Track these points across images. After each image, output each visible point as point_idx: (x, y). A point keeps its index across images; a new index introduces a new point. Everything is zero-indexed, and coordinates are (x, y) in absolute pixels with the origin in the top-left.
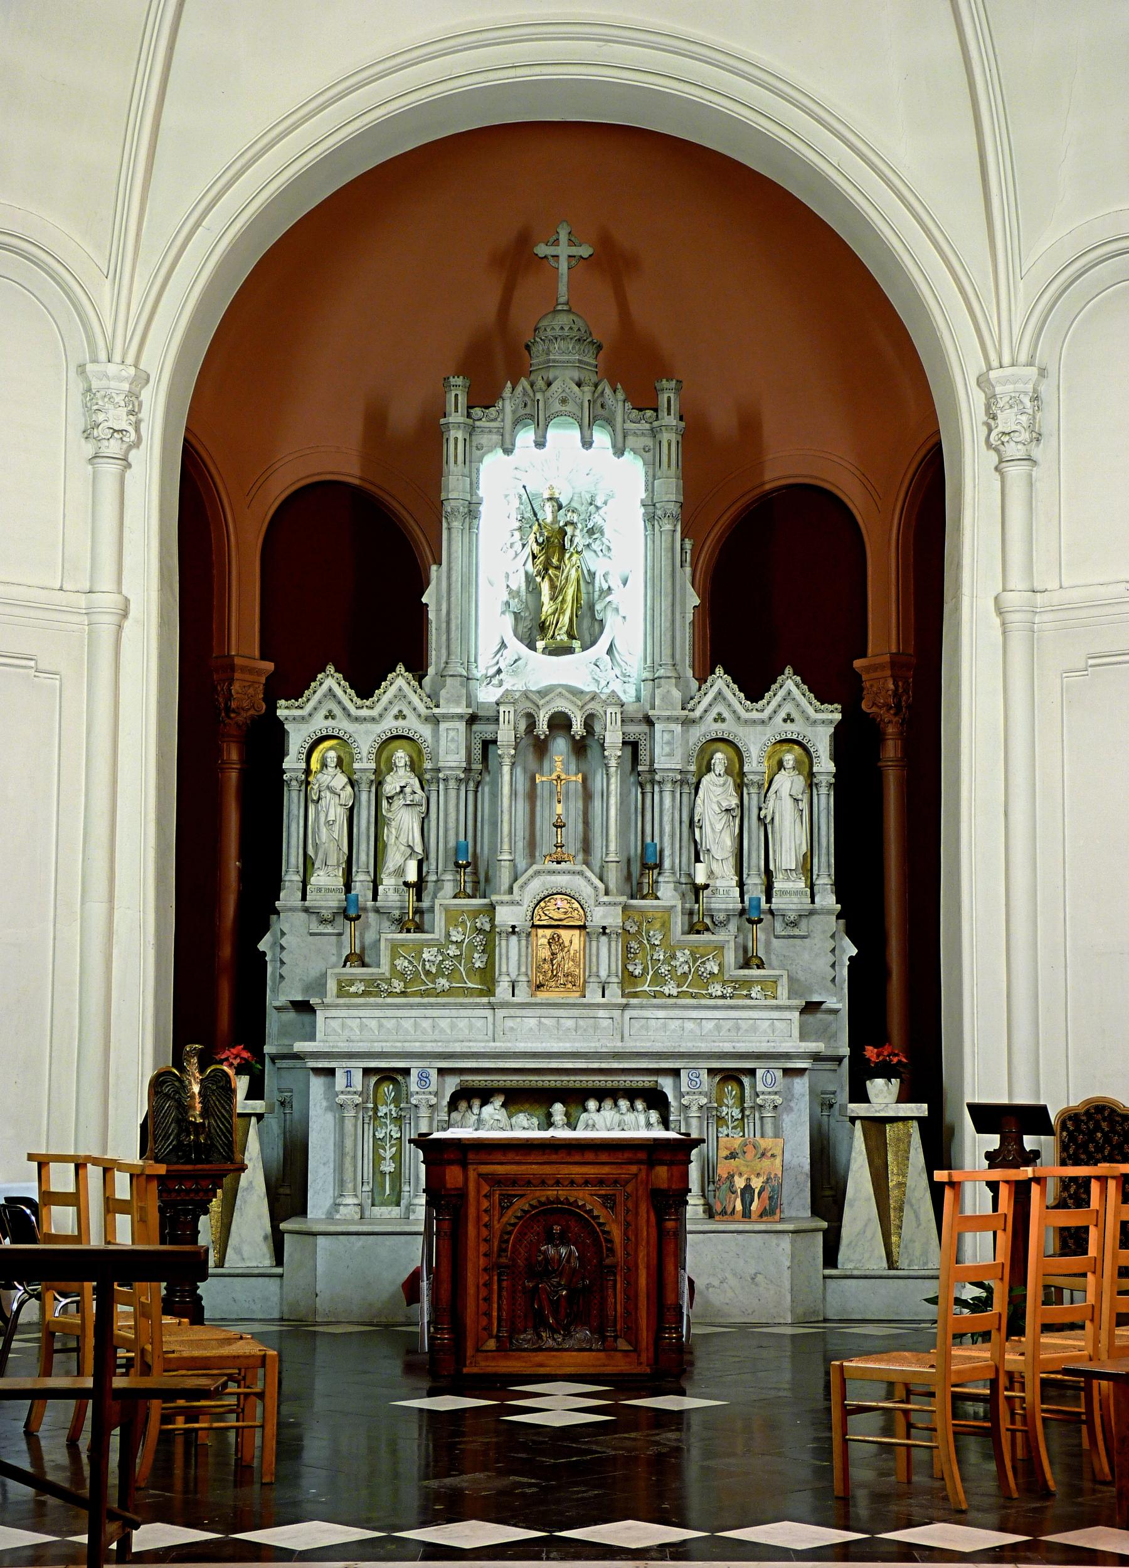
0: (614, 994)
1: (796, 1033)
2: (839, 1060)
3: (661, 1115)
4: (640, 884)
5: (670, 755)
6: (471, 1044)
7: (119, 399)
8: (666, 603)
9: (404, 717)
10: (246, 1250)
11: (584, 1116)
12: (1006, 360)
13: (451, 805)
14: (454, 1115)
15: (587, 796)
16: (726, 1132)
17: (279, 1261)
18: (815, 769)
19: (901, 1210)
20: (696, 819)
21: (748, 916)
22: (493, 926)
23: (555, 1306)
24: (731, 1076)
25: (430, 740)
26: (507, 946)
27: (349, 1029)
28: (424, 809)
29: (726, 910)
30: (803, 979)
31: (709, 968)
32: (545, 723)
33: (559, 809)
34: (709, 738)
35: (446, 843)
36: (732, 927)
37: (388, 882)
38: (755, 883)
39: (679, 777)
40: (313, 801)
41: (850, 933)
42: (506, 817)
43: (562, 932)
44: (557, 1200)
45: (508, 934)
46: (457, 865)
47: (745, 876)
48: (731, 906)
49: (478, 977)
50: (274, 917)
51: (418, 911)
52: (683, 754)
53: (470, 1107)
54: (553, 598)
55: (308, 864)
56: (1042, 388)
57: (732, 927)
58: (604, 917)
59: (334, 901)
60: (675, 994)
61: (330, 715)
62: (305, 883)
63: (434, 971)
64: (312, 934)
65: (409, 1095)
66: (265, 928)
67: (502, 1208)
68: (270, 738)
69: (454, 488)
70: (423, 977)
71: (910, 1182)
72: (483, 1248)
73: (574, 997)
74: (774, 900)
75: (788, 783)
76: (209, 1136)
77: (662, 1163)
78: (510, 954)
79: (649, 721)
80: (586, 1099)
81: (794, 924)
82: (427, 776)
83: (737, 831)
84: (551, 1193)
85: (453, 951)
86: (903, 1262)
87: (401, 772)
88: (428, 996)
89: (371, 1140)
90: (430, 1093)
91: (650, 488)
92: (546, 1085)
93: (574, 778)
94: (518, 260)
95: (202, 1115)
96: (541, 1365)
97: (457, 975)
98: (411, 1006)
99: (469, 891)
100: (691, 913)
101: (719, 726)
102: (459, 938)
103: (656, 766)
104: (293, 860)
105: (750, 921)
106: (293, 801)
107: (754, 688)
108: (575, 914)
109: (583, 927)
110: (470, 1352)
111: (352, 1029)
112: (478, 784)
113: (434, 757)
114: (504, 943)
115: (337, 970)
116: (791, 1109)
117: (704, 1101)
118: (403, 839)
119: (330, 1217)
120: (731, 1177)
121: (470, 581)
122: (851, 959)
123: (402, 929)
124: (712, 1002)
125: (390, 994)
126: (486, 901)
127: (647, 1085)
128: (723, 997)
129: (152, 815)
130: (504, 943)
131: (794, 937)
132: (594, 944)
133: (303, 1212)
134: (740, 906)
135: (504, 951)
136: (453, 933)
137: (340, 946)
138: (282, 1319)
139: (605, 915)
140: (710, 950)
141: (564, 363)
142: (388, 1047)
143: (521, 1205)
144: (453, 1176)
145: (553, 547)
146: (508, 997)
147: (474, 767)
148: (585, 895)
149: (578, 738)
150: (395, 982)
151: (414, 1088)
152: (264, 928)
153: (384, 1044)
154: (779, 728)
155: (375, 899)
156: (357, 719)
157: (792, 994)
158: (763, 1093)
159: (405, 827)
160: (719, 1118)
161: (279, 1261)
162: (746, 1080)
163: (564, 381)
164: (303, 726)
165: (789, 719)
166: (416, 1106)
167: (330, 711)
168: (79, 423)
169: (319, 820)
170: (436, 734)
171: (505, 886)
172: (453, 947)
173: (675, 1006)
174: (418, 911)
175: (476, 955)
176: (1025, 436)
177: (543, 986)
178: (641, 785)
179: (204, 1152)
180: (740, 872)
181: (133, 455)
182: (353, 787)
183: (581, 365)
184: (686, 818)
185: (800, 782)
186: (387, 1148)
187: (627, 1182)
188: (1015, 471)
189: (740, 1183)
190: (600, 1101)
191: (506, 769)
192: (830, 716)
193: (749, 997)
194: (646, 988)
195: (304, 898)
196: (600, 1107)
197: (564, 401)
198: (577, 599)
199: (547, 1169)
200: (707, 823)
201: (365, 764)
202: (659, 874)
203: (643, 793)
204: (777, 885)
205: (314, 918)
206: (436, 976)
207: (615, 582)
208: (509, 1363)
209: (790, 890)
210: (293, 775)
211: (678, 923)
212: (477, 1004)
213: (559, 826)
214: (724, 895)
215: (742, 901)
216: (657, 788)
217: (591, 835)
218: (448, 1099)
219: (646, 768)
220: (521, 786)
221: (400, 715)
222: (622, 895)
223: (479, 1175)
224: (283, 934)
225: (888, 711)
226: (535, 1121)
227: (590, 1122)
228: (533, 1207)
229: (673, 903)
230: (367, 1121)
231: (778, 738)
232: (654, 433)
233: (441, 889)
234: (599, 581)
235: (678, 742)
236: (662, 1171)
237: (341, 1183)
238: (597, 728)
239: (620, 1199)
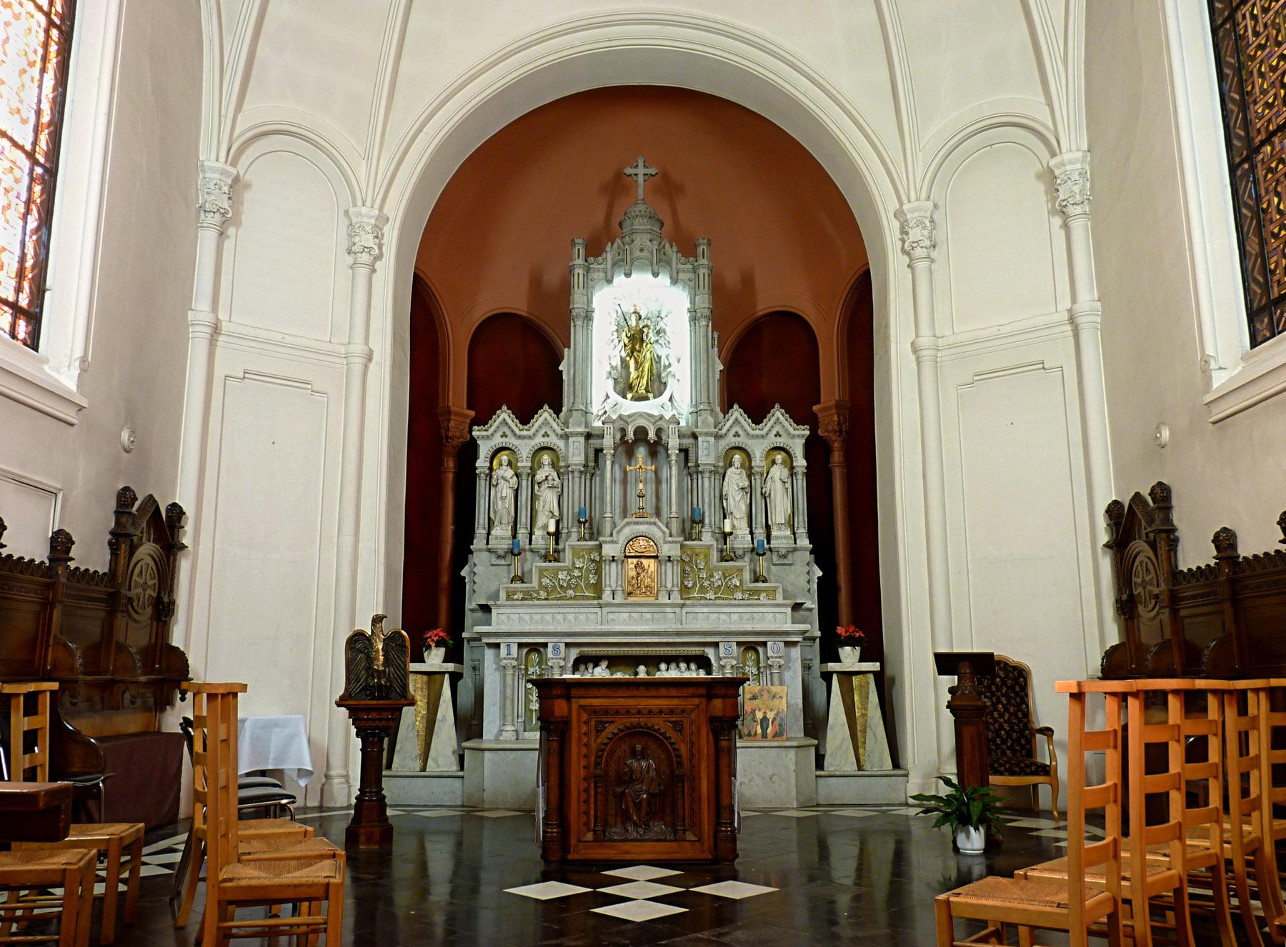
0: (676, 598)
1: (789, 620)
2: (814, 639)
4: (690, 534)
5: (708, 455)
7: (369, 229)
8: (703, 367)
10: (441, 760)
12: (913, 197)
13: (575, 487)
15: (658, 481)
17: (462, 768)
19: (865, 732)
23: (638, 806)
27: (511, 619)
36: (747, 558)
37: (538, 533)
38: (760, 533)
41: (818, 563)
42: (608, 491)
44: (639, 726)
46: (580, 522)
51: (556, 551)
54: (637, 369)
55: (490, 523)
56: (935, 216)
57: (747, 558)
59: (505, 545)
61: (504, 435)
62: (489, 534)
65: (547, 660)
66: (465, 562)
67: (597, 731)
68: (471, 448)
69: (578, 301)
71: (870, 713)
72: (583, 762)
73: (651, 600)
75: (779, 472)
76: (388, 680)
77: (718, 697)
79: (695, 436)
81: (784, 557)
84: (634, 720)
85: (576, 573)
86: (867, 766)
87: (546, 468)
91: (693, 302)
94: (618, 186)
95: (383, 665)
96: (628, 852)
98: (551, 606)
100: (722, 551)
101: (737, 439)
104: (481, 521)
105: (759, 555)
106: (482, 485)
107: (757, 416)
109: (656, 557)
110: (573, 842)
112: (593, 475)
117: (734, 662)
119: (497, 740)
120: (753, 712)
121: (587, 356)
129: (384, 483)
133: (480, 736)
137: (509, 572)
138: (463, 806)
141: (642, 237)
142: (533, 629)
143: (611, 729)
144: (560, 707)
145: (636, 340)
151: (550, 655)
152: (464, 562)
154: (772, 441)
156: (520, 437)
157: (785, 598)
161: (462, 768)
162: (761, 650)
163: (642, 240)
165: (778, 435)
168: (345, 244)
169: (497, 496)
170: (567, 445)
176: (927, 243)
178: (690, 475)
179: (383, 691)
180: (750, 526)
181: (378, 265)
183: (651, 232)
185: (786, 472)
187: (692, 711)
188: (921, 266)
189: (759, 715)
190: (668, 664)
191: (609, 463)
197: (642, 250)
198: (651, 370)
199: (631, 702)
201: (524, 463)
204: (774, 533)
207: (673, 360)
208: (600, 851)
209: (781, 537)
211: (715, 555)
213: (641, 496)
214: (742, 539)
220: (618, 475)
221: (546, 435)
223: (580, 706)
228: (621, 731)
232: (694, 270)
234: (664, 361)
235: (712, 449)
236: (718, 703)
237: (504, 717)
239: (686, 725)
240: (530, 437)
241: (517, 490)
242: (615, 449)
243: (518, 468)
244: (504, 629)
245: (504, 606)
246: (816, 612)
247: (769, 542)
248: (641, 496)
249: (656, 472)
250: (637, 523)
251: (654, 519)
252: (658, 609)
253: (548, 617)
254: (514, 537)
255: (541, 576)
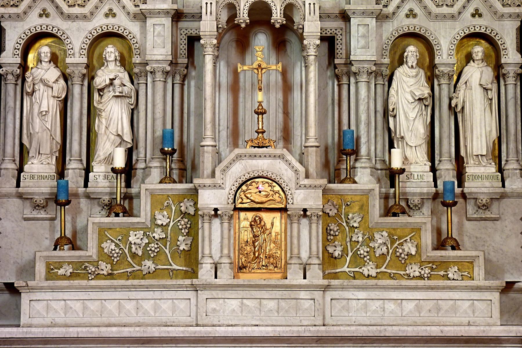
0: (316, 275)
1: (496, 313)
4: (338, 170)
5: (366, 47)
6: (170, 329)
9: (114, 15)
13: (157, 98)
15: (287, 88)
18: (503, 61)
20: (391, 108)
21: (443, 200)
22: (197, 210)
25: (138, 36)
28: (133, 100)
29: (421, 194)
30: (495, 259)
31: (406, 250)
32: (246, 12)
33: (260, 96)
34: (401, 33)
35: (154, 132)
36: (426, 210)
37: (99, 169)
38: (447, 170)
39: (374, 68)
40: (28, 93)
46: (163, 151)
47: (437, 162)
48: (425, 190)
49: (182, 259)
52: (377, 48)
55: (23, 153)
57: (426, 210)
58: (305, 199)
60: (374, 275)
61: (44, 14)
62: (21, 170)
63: (140, 253)
64: (26, 219)
70: (129, 259)
74: (466, 184)
75: (477, 74)
78: (213, 237)
79: (345, 17)
81: (486, 207)
82: (136, 70)
85: (158, 234)
87: (112, 66)
97: (162, 257)
98: (115, 288)
99: (175, 177)
101: (411, 21)
102: (165, 221)
103: (352, 58)
105: (444, 204)
108: (276, 197)
109: (284, 210)
111: (56, 312)
112: (184, 77)
113: (142, 52)
114: (206, 225)
115: (45, 254)
118: (113, 129)
124: (413, 283)
125: (98, 276)
126: (190, 186)
128: (421, 277)
130: (206, 225)
131: (485, 219)
132: (295, 226)
136: (159, 216)
137: (52, 230)
140: (407, 231)
146: (210, 278)
147: (180, 61)
148: (285, 178)
149: (278, 26)
153: (79, 329)
155: (86, 186)
164: (19, 24)
165: (477, 14)
167: (44, 10)
171: (208, 170)
174: (128, 197)
175: (181, 238)
177: (245, 267)
178: (338, 77)
180: (432, 158)
182: (66, 80)
184: (380, 108)
185: (489, 73)
191: (209, 60)
193: (446, 277)
194: (345, 269)
195: (18, 185)
200: (401, 112)
201: (77, 58)
202: (356, 160)
203: (339, 86)
204: (470, 170)
205: (28, 203)
210: (9, 69)
211: (376, 206)
212: (180, 286)
214: (419, 179)
215: (436, 186)
217: (291, 124)
221: (111, 14)
222: (322, 178)
229: (370, 186)
231: (467, 32)
233: (149, 175)
235: (373, 36)
238: (297, 19)
240: (85, 17)
241: (65, 101)
242: (220, 38)
247: (461, 184)
249: (284, 73)
250: (254, 156)
252: (287, 294)
253: (111, 306)
254: (61, 173)
255: (102, 237)
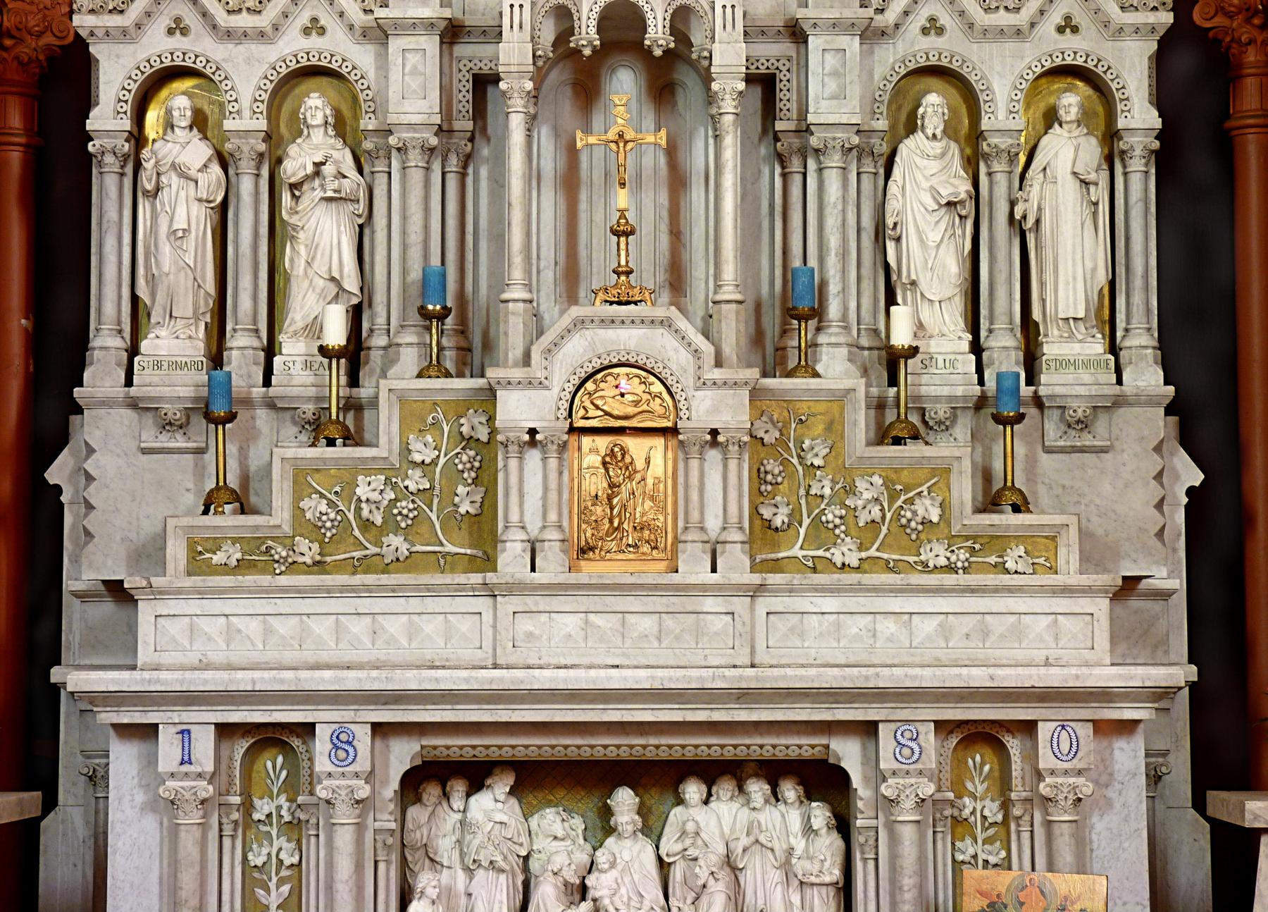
3: (836, 815)
4: (781, 350)
5: (840, 96)
9: (322, 31)
11: (677, 811)
14: (413, 812)
15: (678, 181)
16: (971, 851)
18: (1121, 123)
20: (890, 222)
21: (997, 411)
22: (493, 432)
24: (982, 735)
25: (371, 75)
26: (521, 469)
28: (362, 207)
29: (951, 398)
30: (1100, 532)
31: (921, 512)
33: (622, 199)
34: (912, 66)
35: (405, 272)
36: (962, 431)
37: (293, 348)
38: (1004, 347)
39: (856, 140)
41: (1187, 441)
43: (630, 442)
45: (522, 446)
46: (422, 311)
47: (983, 334)
48: (959, 391)
49: (464, 533)
50: (75, 419)
51: (353, 406)
52: (862, 98)
53: (446, 795)
57: (962, 431)
58: (715, 410)
60: (855, 563)
62: (133, 351)
63: (378, 520)
64: (145, 451)
65: (313, 779)
66: (60, 440)
70: (357, 533)
75: (1068, 151)
80: (681, 779)
81: (1083, 425)
82: (368, 145)
83: (968, 246)
85: (416, 480)
87: (318, 136)
88: (367, 571)
89: (238, 870)
90: (357, 775)
92: (599, 754)
93: (651, 139)
97: (424, 529)
98: (329, 592)
99: (449, 364)
101: (932, 41)
104: (109, 308)
105: (998, 419)
106: (108, 193)
108: (656, 405)
109: (670, 432)
112: (467, 160)
114: (513, 463)
115: (186, 521)
116: (1109, 804)
117: (928, 789)
118: (320, 267)
122: (1191, 491)
123: (316, 438)
125: (293, 568)
126: (479, 382)
127: (807, 754)
128: (950, 568)
130: (513, 463)
131: (1082, 450)
132: (694, 464)
134: (977, 390)
135: (514, 479)
136: (415, 445)
137: (200, 472)
139: (717, 406)
140: (922, 474)
148: (674, 367)
149: (658, 52)
150: (303, 544)
151: (322, 764)
155: (267, 382)
156: (229, 34)
158: (1052, 772)
159: (325, 242)
160: (957, 821)
162: (1014, 745)
165: (1068, 26)
166: (328, 802)
167: (178, 20)
171: (516, 352)
172: (416, 474)
173: (859, 589)
175: (461, 490)
177: (592, 549)
178: (781, 159)
180: (974, 328)
182: (224, 166)
185: (1091, 150)
186: (272, 885)
190: (710, 782)
191: (517, 123)
192: (1151, 18)
193: (1001, 568)
194: (796, 551)
195: (129, 382)
196: (710, 794)
200: (912, 230)
201: (245, 121)
202: (818, 329)
204: (1051, 349)
205: (149, 419)
206: (383, 530)
210: (108, 143)
211: (859, 424)
212: (461, 587)
213: (623, 232)
214: (946, 371)
215: (981, 382)
216: (812, 165)
217: (685, 257)
218: (395, 784)
219: (791, 126)
220: (549, 159)
222: (749, 366)
224: (90, 451)
225: (1248, 21)
226: (578, 823)
227: (690, 827)
230: (228, 830)
231: (1048, 65)
235: (853, 75)
238: (697, 38)
241: (224, 205)
242: (539, 77)
243: (224, 136)
244: (169, 681)
245: (178, 592)
246: (1181, 601)
248: (623, 232)
249: (671, 151)
251: (662, 311)
252: (677, 603)
254: (216, 359)
255: (300, 489)
